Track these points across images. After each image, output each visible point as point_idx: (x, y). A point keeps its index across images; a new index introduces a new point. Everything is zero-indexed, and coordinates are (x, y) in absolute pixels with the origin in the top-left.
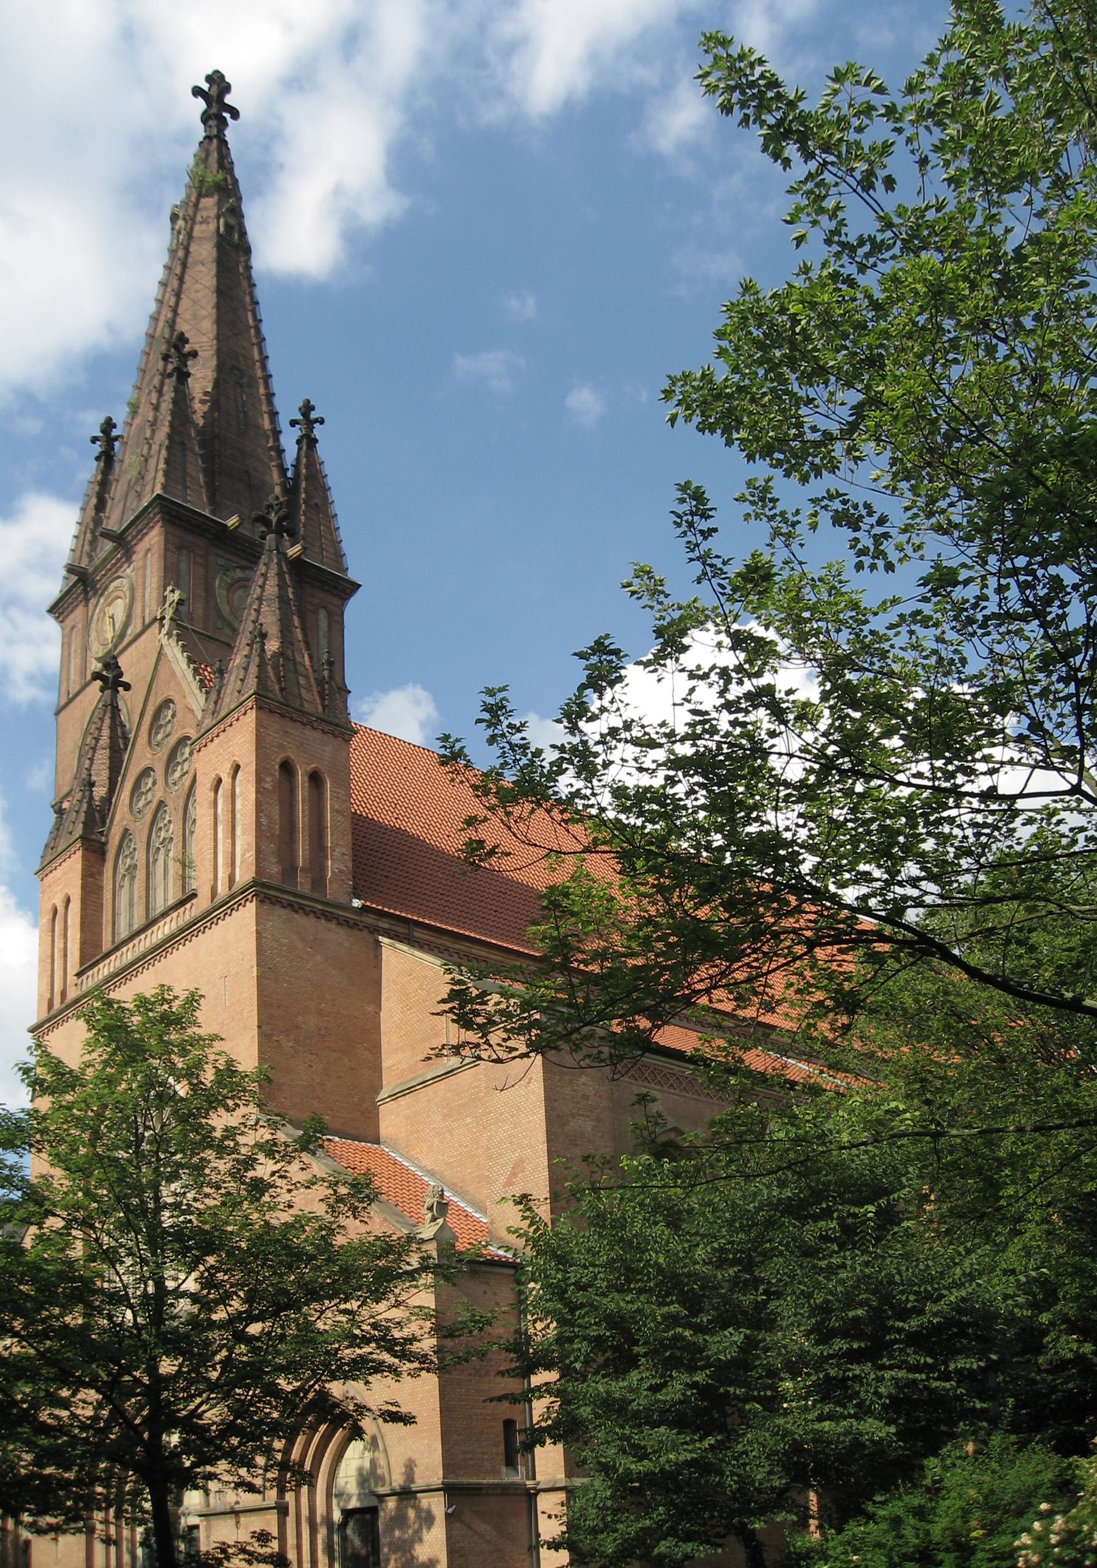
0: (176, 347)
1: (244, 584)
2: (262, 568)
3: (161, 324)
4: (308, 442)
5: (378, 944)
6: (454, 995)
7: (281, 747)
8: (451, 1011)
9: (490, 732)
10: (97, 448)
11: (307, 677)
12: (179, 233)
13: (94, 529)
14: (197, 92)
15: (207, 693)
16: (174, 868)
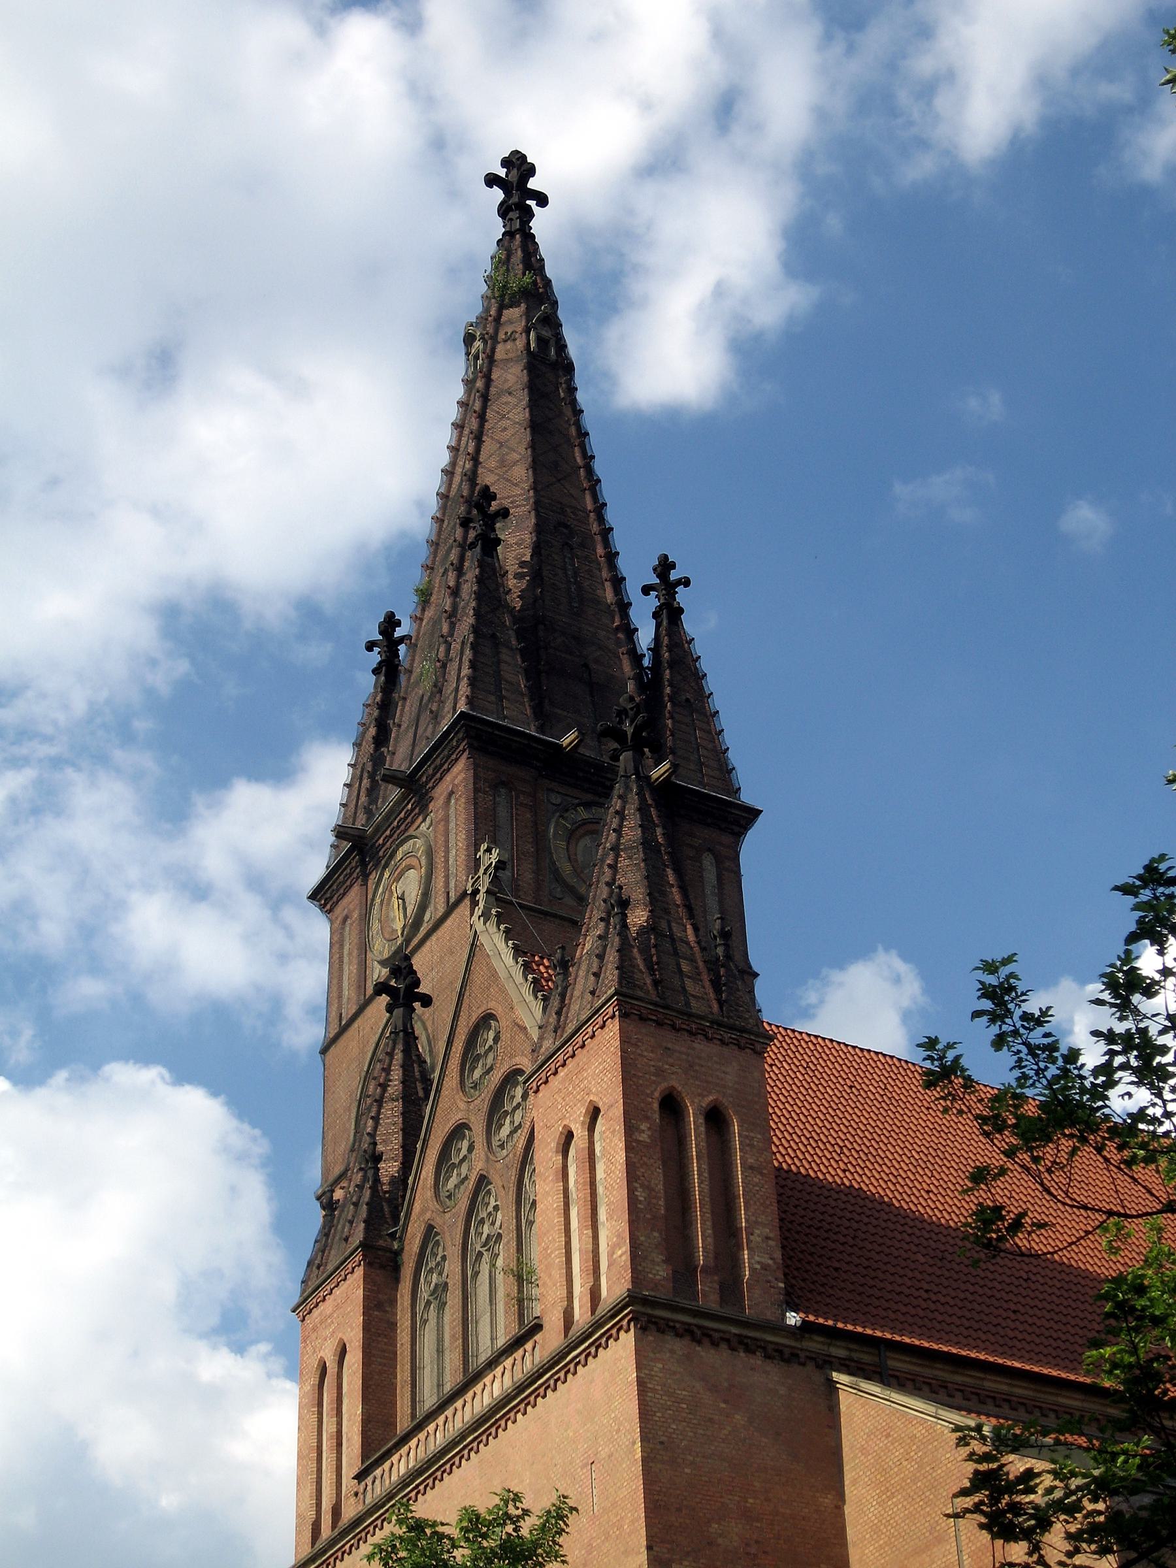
0: (479, 506)
1: (593, 828)
2: (617, 804)
3: (457, 479)
4: (669, 615)
5: (832, 1388)
6: (980, 1481)
7: (660, 1072)
8: (976, 1509)
9: (995, 1029)
10: (375, 657)
11: (692, 960)
12: (476, 357)
13: (372, 773)
14: (492, 180)
15: (545, 999)
16: (505, 1286)
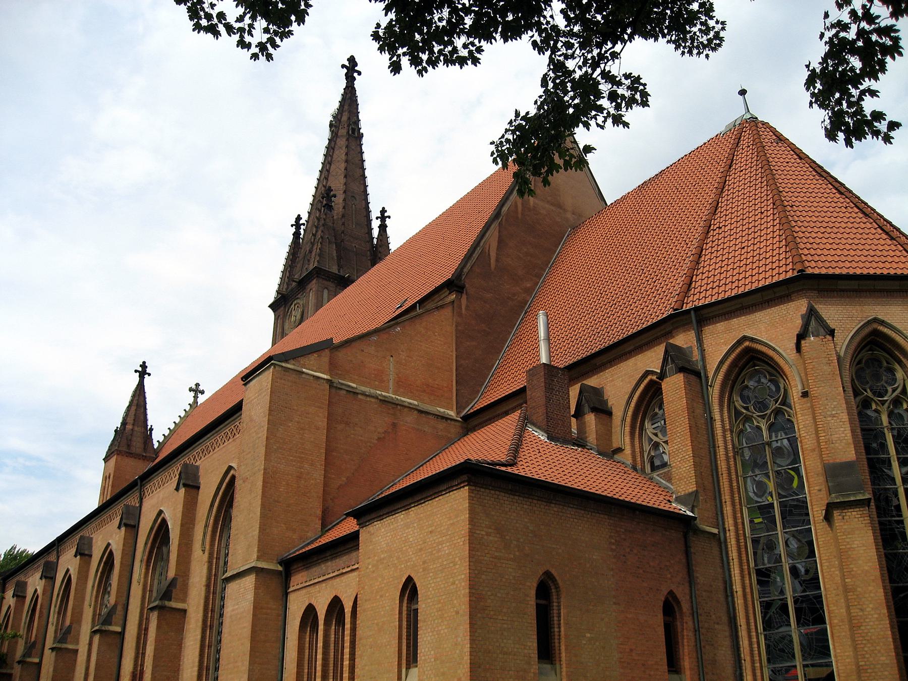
4: (383, 227)
